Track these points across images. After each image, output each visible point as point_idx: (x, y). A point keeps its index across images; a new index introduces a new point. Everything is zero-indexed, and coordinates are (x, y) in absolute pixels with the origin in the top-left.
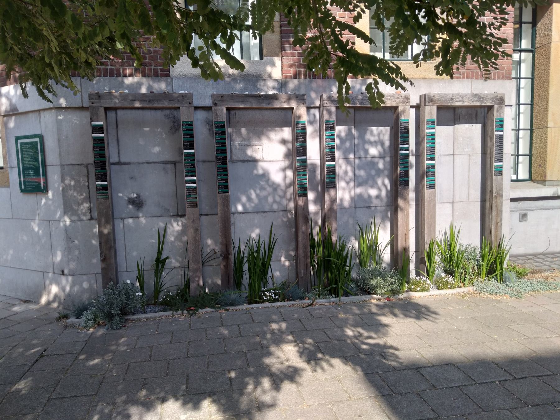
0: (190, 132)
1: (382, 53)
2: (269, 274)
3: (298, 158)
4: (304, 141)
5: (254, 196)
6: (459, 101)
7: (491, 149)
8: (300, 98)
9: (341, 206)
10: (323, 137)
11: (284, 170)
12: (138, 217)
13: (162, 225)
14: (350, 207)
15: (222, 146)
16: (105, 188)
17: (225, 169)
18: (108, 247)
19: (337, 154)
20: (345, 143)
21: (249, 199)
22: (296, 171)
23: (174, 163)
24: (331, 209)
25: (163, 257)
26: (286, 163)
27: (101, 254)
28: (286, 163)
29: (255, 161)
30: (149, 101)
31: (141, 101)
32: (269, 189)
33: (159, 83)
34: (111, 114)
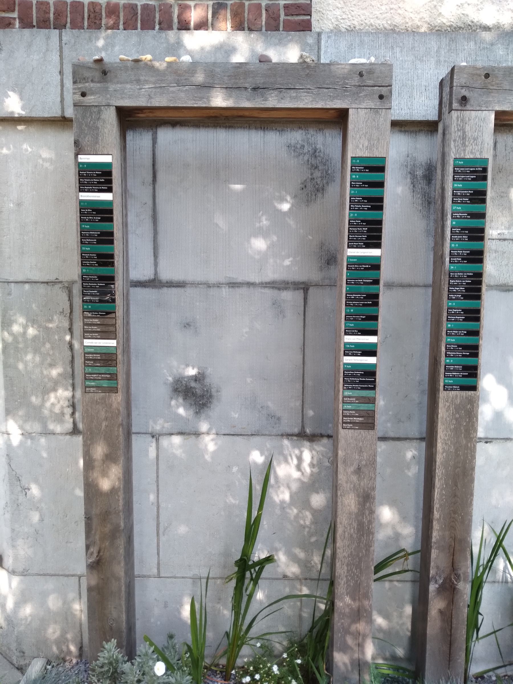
0: (373, 192)
12: (197, 434)
13: (257, 457)
15: (471, 239)
16: (107, 358)
17: (474, 315)
18: (109, 529)
23: (304, 288)
25: (259, 553)
27: (88, 547)
30: (255, 89)
31: (230, 89)
33: (280, 49)
34: (140, 141)
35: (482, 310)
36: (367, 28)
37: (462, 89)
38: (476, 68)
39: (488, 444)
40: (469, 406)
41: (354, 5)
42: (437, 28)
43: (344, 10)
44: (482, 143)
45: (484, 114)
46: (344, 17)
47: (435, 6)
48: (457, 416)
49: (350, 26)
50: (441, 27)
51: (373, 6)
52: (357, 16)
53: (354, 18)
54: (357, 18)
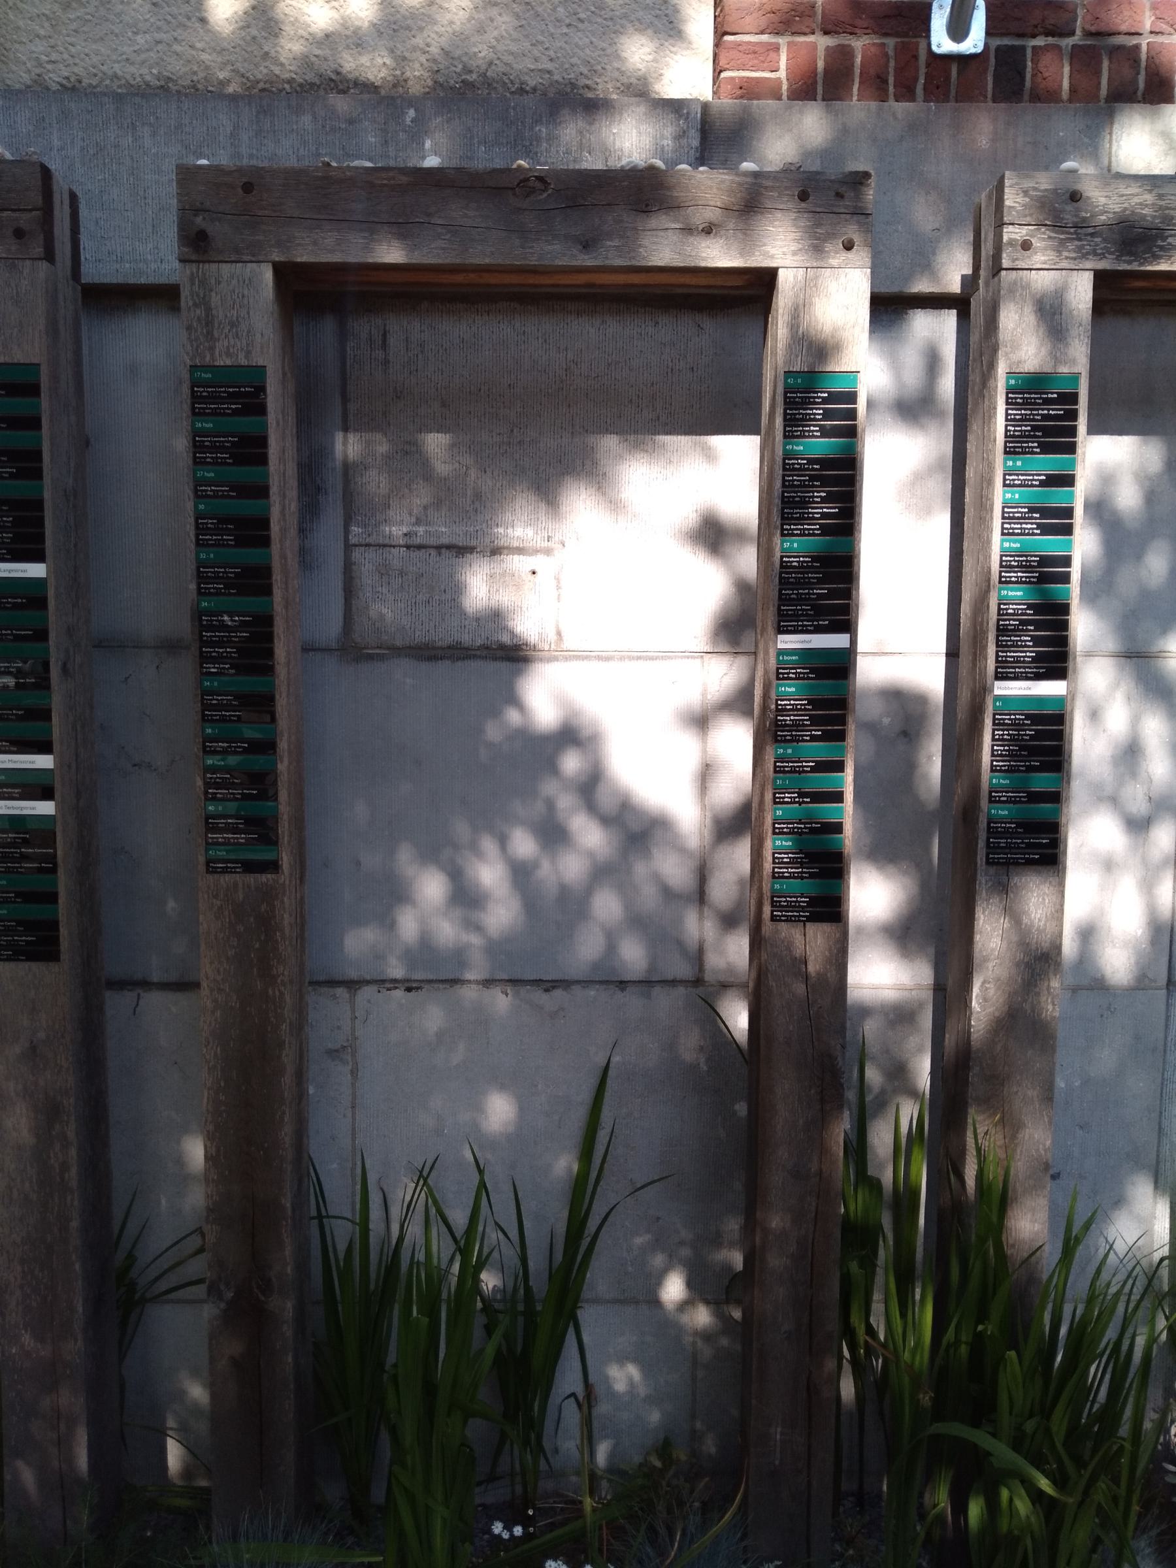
2: (568, 1380)
3: (789, 642)
4: (846, 522)
5: (490, 874)
8: (830, 199)
9: (1091, 984)
10: (984, 506)
11: (701, 721)
14: (1142, 982)
15: (241, 542)
19: (1084, 626)
20: (1139, 557)
21: (465, 897)
22: (772, 732)
24: (1021, 1021)
26: (720, 675)
28: (720, 675)
29: (514, 656)
32: (590, 836)
35: (277, 697)
36: (108, 82)
37: (195, 215)
38: (222, 170)
39: (413, 993)
40: (264, 907)
41: (76, 31)
42: (261, 85)
43: (52, 41)
44: (249, 332)
45: (248, 270)
46: (54, 57)
47: (254, 38)
48: (240, 928)
49: (67, 78)
50: (271, 83)
51: (116, 36)
52: (83, 56)
53: (77, 61)
54: (82, 60)
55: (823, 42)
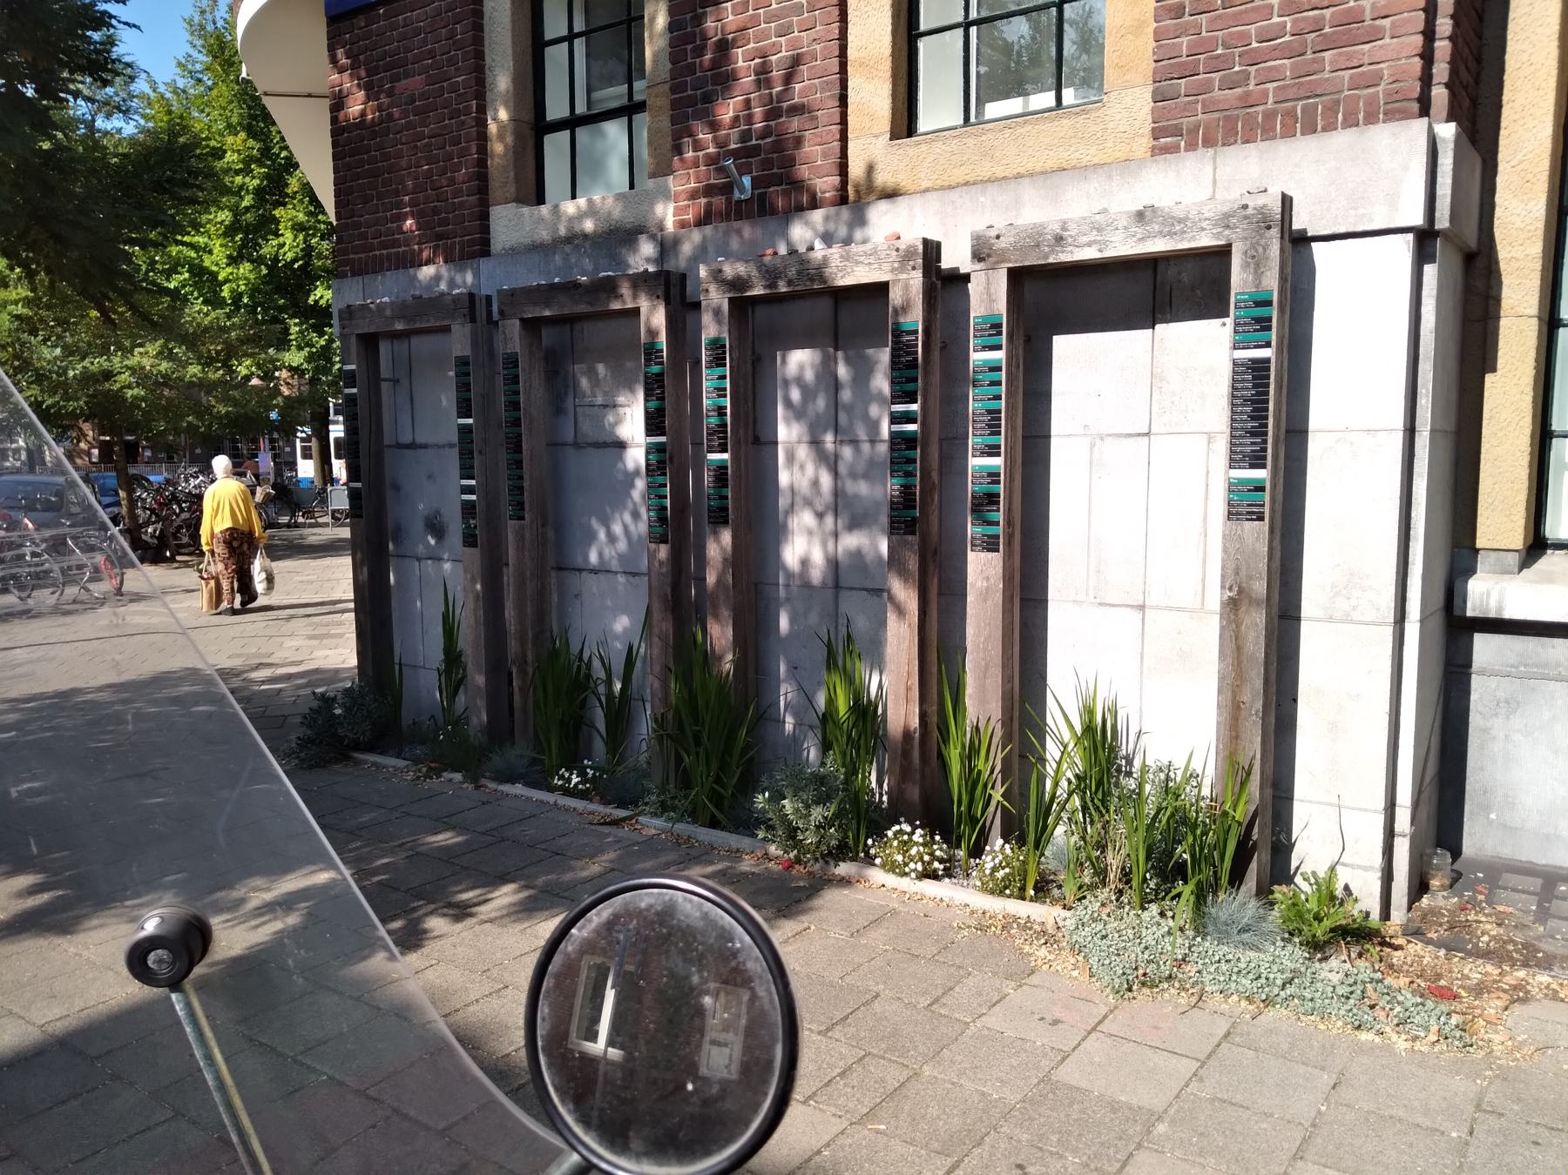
1: (1053, 94)
5: (617, 529)
6: (1089, 244)
7: (1271, 418)
14: (824, 586)
21: (612, 539)
55: (703, 201)
